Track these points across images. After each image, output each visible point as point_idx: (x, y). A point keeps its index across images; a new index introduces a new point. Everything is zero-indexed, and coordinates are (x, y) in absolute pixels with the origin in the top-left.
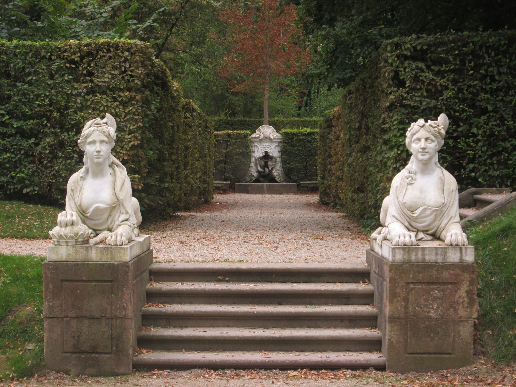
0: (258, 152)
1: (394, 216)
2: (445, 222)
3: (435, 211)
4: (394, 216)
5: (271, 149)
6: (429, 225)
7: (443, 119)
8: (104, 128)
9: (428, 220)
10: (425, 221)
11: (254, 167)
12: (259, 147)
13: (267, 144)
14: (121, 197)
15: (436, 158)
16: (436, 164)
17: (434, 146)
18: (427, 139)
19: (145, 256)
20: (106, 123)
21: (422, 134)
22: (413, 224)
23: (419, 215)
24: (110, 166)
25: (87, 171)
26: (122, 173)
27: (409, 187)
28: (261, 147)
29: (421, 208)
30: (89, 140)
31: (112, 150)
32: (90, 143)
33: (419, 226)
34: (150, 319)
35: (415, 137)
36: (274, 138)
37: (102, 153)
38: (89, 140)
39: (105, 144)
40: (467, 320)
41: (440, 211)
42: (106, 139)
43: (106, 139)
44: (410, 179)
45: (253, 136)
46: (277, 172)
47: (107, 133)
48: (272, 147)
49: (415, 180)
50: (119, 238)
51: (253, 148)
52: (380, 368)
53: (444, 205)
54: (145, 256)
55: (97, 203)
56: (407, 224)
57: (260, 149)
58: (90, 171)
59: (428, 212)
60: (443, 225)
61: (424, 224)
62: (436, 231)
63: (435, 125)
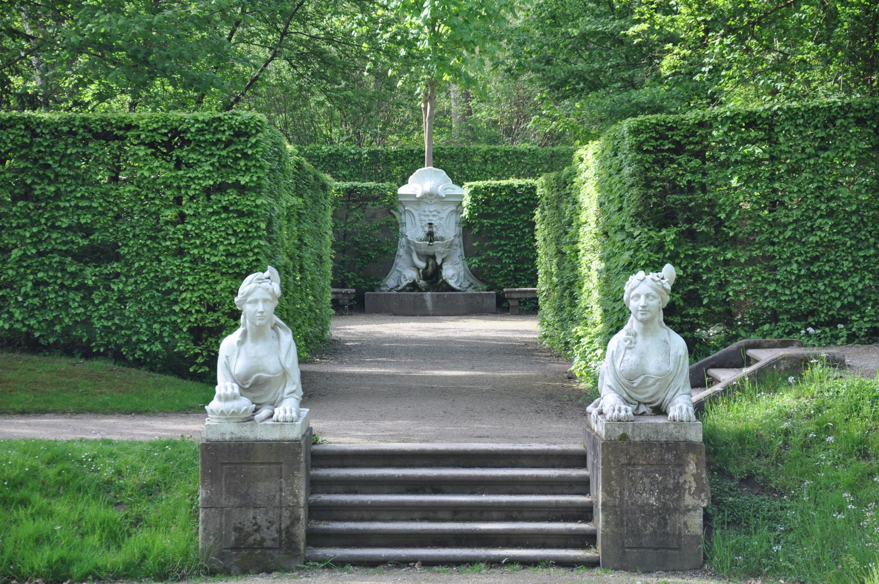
0: (414, 225)
1: (609, 386)
2: (671, 393)
3: (658, 380)
4: (609, 386)
5: (441, 219)
6: (652, 396)
7: (669, 271)
8: (266, 284)
9: (651, 391)
10: (647, 392)
11: (405, 256)
12: (415, 213)
13: (432, 208)
14: (288, 366)
15: (661, 317)
16: (660, 322)
17: (657, 304)
18: (647, 296)
19: (310, 437)
20: (269, 278)
21: (644, 288)
22: (633, 395)
23: (640, 384)
24: (273, 328)
25: (245, 334)
26: (287, 337)
27: (628, 351)
28: (420, 215)
29: (642, 377)
30: (249, 299)
31: (276, 309)
32: (250, 302)
33: (641, 397)
34: (316, 511)
35: (633, 293)
36: (447, 196)
37: (265, 314)
38: (249, 299)
39: (268, 303)
40: (695, 509)
41: (666, 380)
42: (269, 297)
43: (269, 297)
44: (628, 342)
45: (402, 190)
46: (453, 273)
47: (271, 290)
48: (444, 215)
49: (635, 343)
50: (288, 414)
51: (403, 217)
52: (592, 564)
53: (668, 374)
54: (310, 437)
55: (258, 371)
56: (625, 395)
57: (417, 218)
58: (249, 334)
59: (651, 381)
60: (669, 397)
61: (647, 396)
62: (661, 404)
63: (657, 279)
